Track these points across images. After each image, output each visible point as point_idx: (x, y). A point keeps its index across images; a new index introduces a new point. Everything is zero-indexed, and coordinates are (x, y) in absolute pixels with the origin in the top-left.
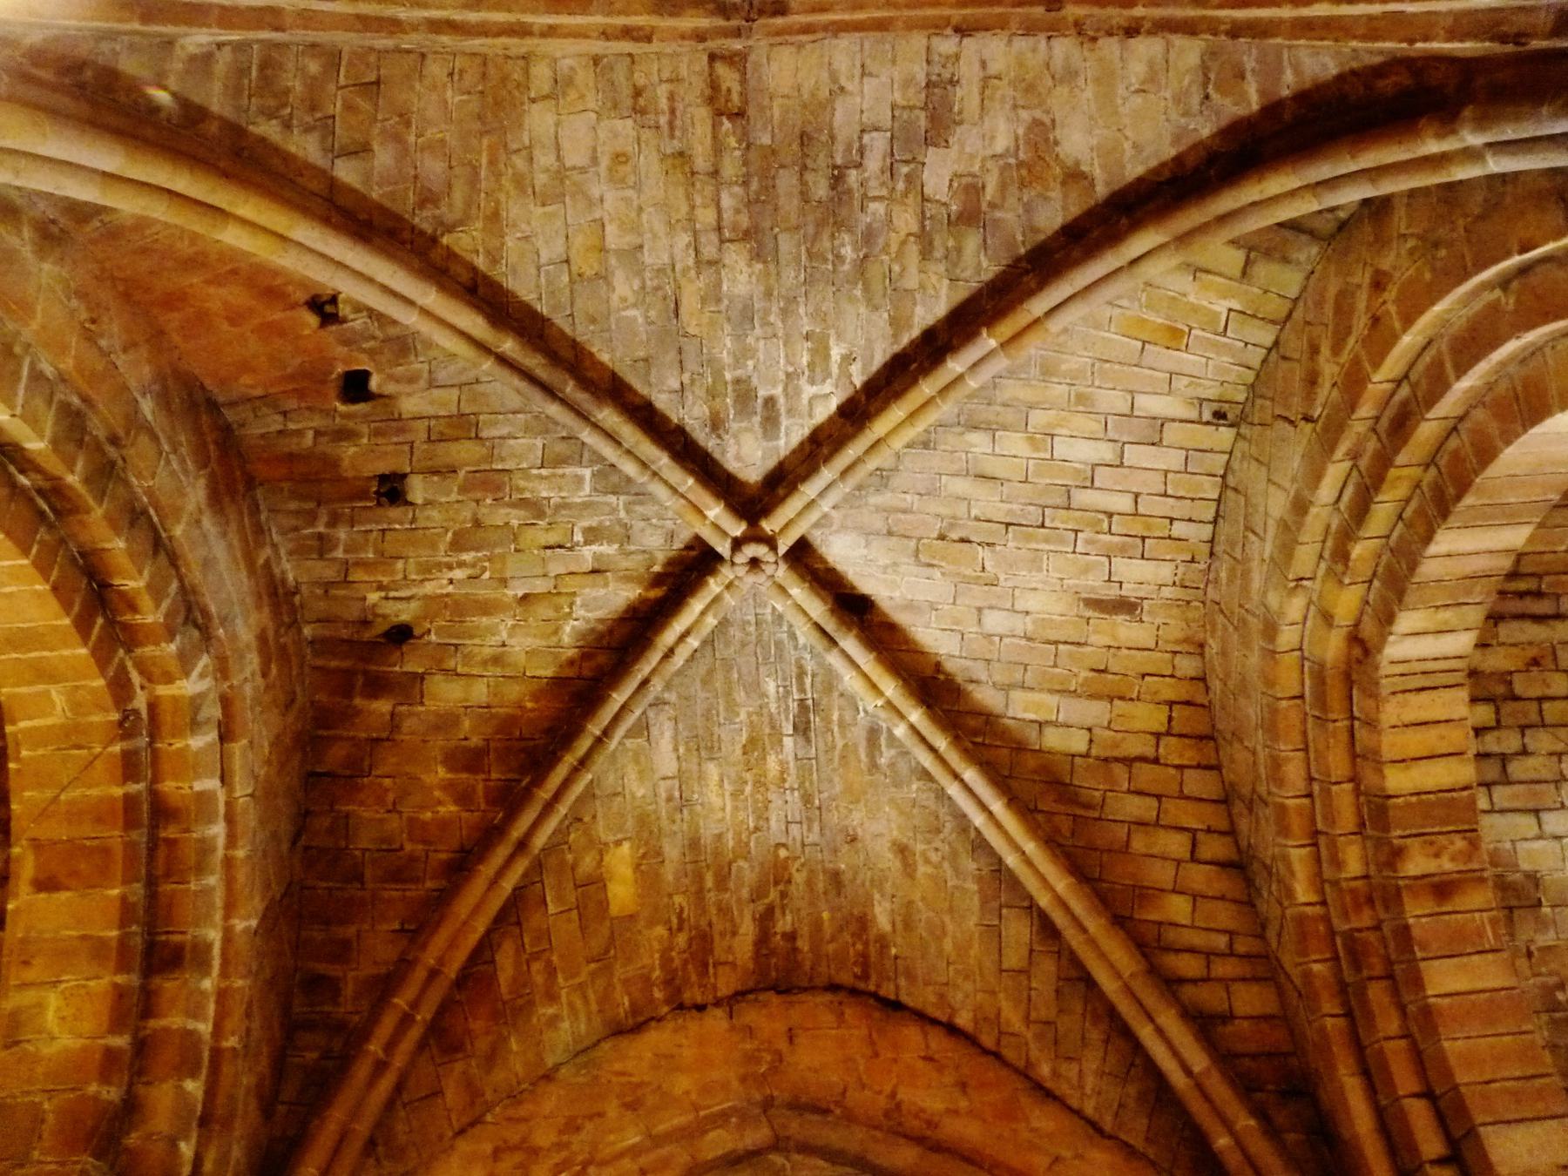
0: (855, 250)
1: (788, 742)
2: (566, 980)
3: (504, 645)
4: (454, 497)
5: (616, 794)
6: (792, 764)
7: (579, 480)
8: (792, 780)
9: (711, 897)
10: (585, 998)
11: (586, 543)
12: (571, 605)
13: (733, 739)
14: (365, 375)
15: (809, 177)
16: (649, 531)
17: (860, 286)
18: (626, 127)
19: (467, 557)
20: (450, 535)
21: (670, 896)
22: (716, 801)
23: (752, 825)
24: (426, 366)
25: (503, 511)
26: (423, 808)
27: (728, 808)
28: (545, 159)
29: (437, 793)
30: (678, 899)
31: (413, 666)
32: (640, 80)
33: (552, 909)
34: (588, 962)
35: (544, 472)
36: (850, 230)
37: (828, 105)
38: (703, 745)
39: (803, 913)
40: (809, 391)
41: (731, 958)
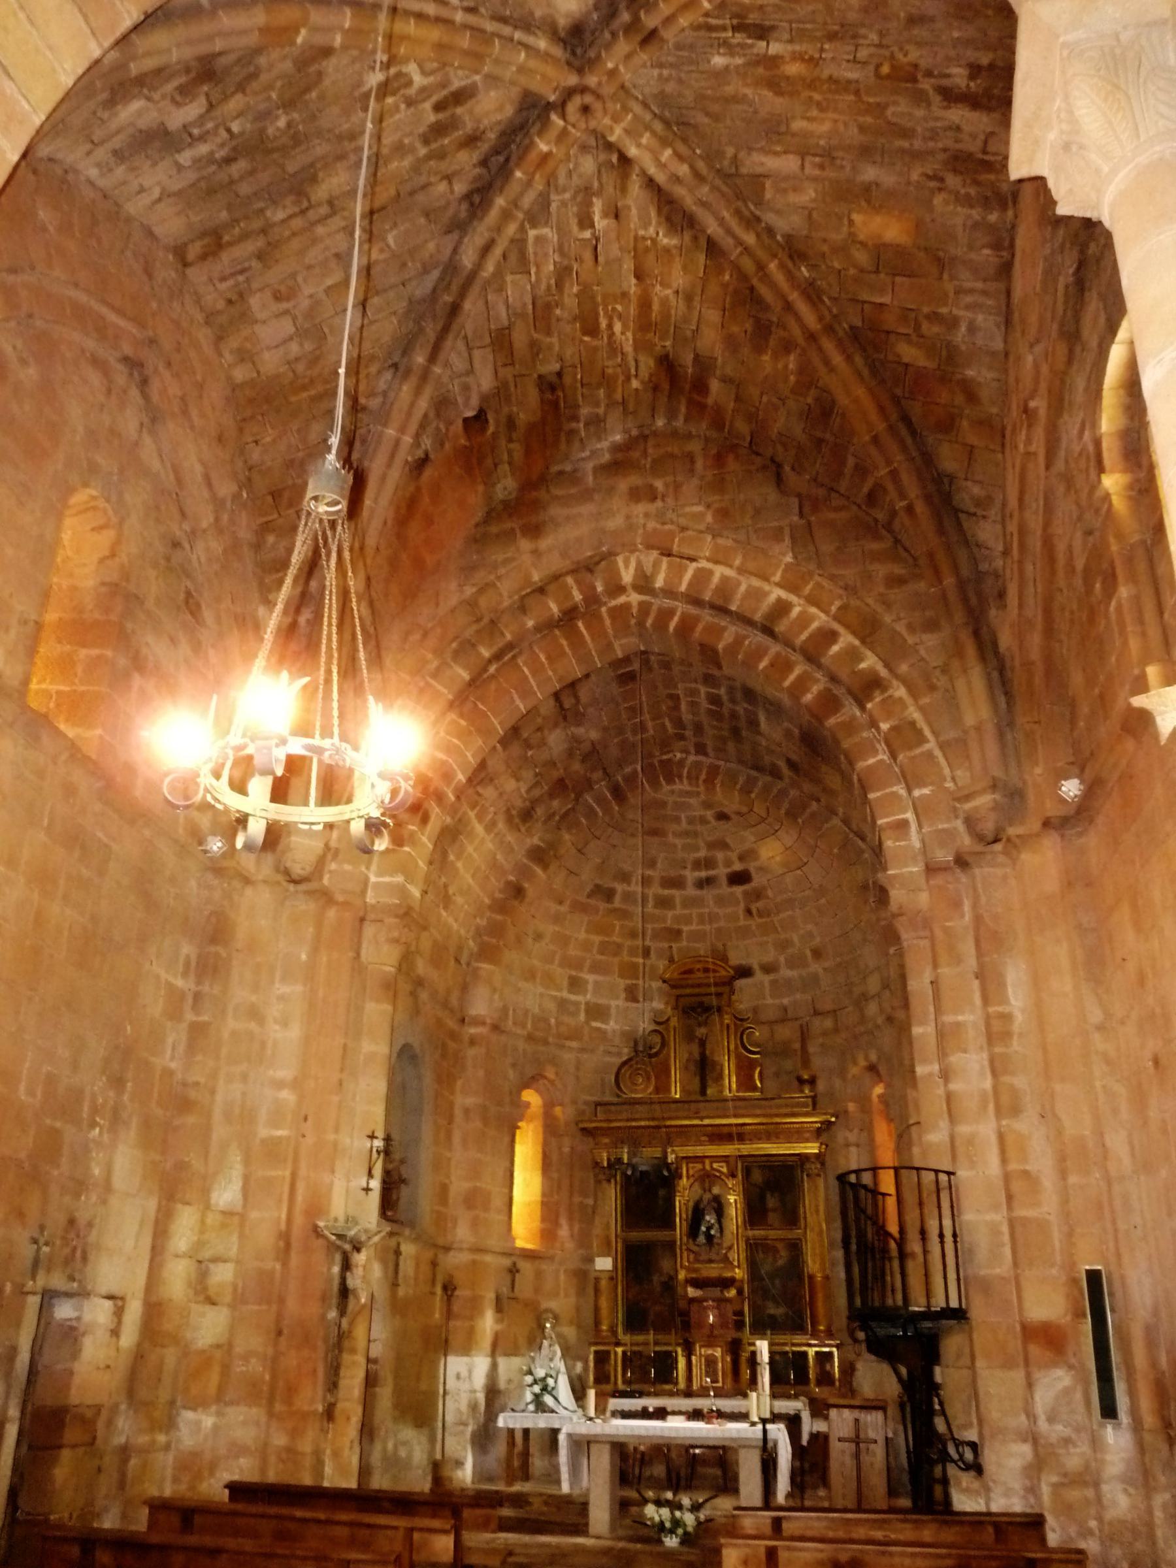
0: (277, 117)
1: (775, 48)
2: (946, 305)
3: (677, 292)
4: (554, 340)
5: (810, 216)
6: (797, 48)
7: (539, 240)
8: (810, 49)
9: (918, 144)
10: (971, 291)
11: (592, 226)
12: (644, 238)
13: (769, 102)
14: (466, 420)
15: (236, 176)
16: (582, 170)
17: (307, 97)
18: (254, 302)
19: (603, 323)
20: (586, 338)
21: (909, 183)
22: (826, 127)
23: (852, 97)
24: (456, 382)
25: (567, 300)
26: (786, 380)
27: (835, 116)
28: (294, 348)
29: (780, 366)
30: (915, 176)
31: (688, 359)
32: (221, 305)
33: (886, 299)
34: (941, 278)
35: (533, 271)
36: (262, 131)
37: (179, 194)
38: (774, 131)
39: (952, 53)
40: (418, 80)
41: (982, 137)
